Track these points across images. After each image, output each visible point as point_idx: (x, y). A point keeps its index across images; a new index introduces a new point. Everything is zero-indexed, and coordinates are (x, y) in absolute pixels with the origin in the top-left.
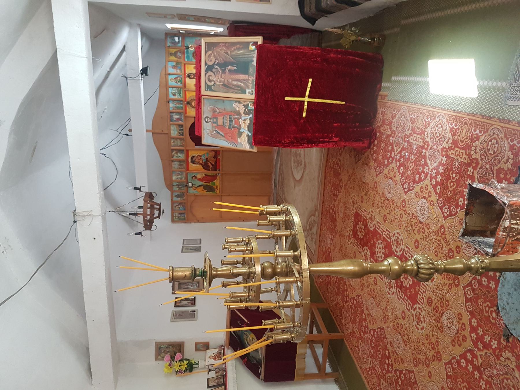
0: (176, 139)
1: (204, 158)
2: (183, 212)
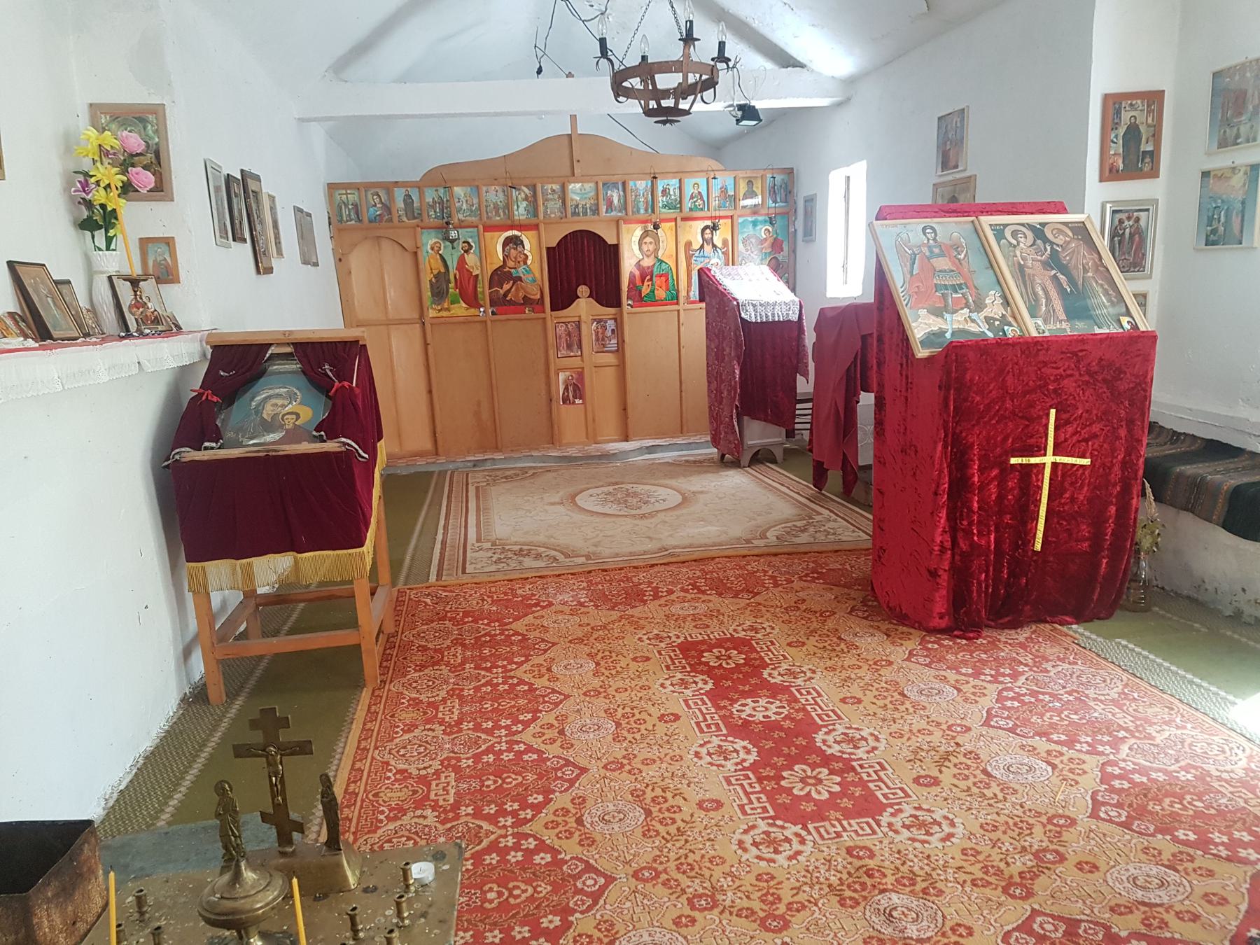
0: (564, 200)
1: (521, 271)
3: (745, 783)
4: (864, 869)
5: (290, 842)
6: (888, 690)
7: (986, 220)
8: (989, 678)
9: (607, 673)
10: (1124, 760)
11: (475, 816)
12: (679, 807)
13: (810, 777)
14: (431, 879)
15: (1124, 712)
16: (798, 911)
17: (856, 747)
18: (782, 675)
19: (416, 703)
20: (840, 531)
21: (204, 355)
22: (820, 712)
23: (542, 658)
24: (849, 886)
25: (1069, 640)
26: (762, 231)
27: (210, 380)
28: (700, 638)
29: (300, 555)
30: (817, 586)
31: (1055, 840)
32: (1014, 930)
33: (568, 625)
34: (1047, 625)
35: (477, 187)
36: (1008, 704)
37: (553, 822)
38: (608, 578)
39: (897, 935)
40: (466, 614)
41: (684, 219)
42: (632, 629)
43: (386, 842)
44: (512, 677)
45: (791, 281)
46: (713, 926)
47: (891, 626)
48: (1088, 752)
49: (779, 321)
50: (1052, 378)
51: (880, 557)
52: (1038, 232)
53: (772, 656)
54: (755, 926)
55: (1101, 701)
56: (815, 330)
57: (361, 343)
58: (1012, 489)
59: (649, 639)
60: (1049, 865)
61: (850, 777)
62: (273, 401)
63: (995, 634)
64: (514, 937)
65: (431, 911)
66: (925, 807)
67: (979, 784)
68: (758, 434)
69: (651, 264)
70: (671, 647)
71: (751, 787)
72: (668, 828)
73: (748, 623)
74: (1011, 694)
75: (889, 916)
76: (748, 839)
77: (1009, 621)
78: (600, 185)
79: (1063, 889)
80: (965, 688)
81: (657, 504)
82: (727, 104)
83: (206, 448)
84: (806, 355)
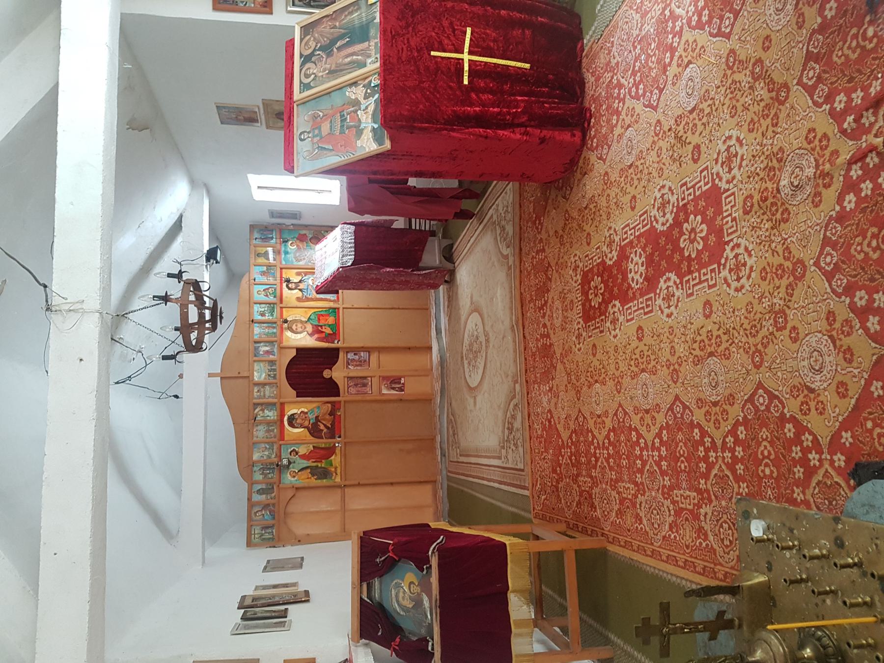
0: (263, 385)
1: (312, 416)
2: (272, 522)
3: (692, 283)
4: (761, 203)
5: (731, 621)
6: (627, 177)
7: (297, 96)
8: (621, 104)
9: (603, 376)
10: (688, 12)
11: (707, 478)
12: (708, 332)
13: (690, 237)
14: (764, 523)
15: (651, 10)
16: (790, 253)
17: (669, 202)
18: (612, 251)
19: (620, 513)
20: (505, 203)
21: (366, 645)
22: (641, 226)
23: (590, 421)
24: (773, 215)
25: (595, 46)
26: (292, 248)
27: (384, 642)
28: (580, 307)
29: (510, 588)
30: (546, 222)
31: (745, 65)
32: (812, 99)
33: (565, 400)
34: (584, 61)
35: (253, 443)
36: (641, 92)
37: (714, 423)
38: (532, 369)
39: (812, 182)
40: (554, 471)
41: (281, 301)
42: (571, 355)
43: (723, 543)
44: (604, 443)
45: (326, 229)
46: (799, 314)
47: (578, 171)
48: (680, 38)
49: (355, 239)
50: (409, 53)
51: (528, 177)
52: (307, 59)
53: (597, 257)
54: (800, 284)
55: (642, 26)
56: (363, 215)
57: (362, 535)
58: (485, 83)
59: (579, 344)
60: (764, 70)
61: (691, 208)
62: (400, 599)
63: (588, 98)
64: (800, 457)
65: (788, 524)
66: (715, 156)
67: (700, 117)
68: (432, 257)
69: (311, 326)
70: (586, 328)
71: (695, 279)
72: (723, 341)
73: (571, 272)
74: (634, 89)
75: (798, 188)
76: (734, 284)
77: (579, 88)
78: (255, 358)
79: (783, 61)
80: (627, 122)
81: (479, 331)
82: (205, 269)
83: (433, 649)
84: (378, 221)
